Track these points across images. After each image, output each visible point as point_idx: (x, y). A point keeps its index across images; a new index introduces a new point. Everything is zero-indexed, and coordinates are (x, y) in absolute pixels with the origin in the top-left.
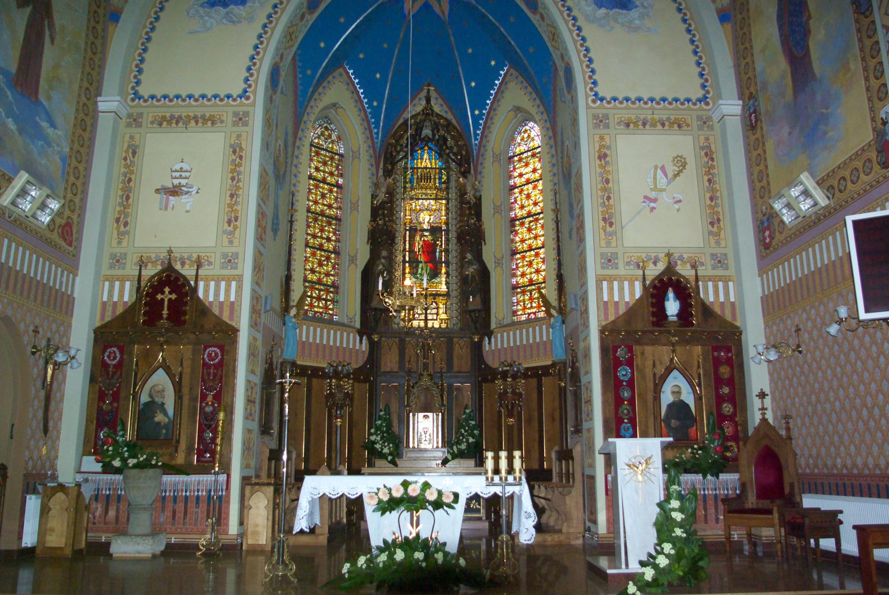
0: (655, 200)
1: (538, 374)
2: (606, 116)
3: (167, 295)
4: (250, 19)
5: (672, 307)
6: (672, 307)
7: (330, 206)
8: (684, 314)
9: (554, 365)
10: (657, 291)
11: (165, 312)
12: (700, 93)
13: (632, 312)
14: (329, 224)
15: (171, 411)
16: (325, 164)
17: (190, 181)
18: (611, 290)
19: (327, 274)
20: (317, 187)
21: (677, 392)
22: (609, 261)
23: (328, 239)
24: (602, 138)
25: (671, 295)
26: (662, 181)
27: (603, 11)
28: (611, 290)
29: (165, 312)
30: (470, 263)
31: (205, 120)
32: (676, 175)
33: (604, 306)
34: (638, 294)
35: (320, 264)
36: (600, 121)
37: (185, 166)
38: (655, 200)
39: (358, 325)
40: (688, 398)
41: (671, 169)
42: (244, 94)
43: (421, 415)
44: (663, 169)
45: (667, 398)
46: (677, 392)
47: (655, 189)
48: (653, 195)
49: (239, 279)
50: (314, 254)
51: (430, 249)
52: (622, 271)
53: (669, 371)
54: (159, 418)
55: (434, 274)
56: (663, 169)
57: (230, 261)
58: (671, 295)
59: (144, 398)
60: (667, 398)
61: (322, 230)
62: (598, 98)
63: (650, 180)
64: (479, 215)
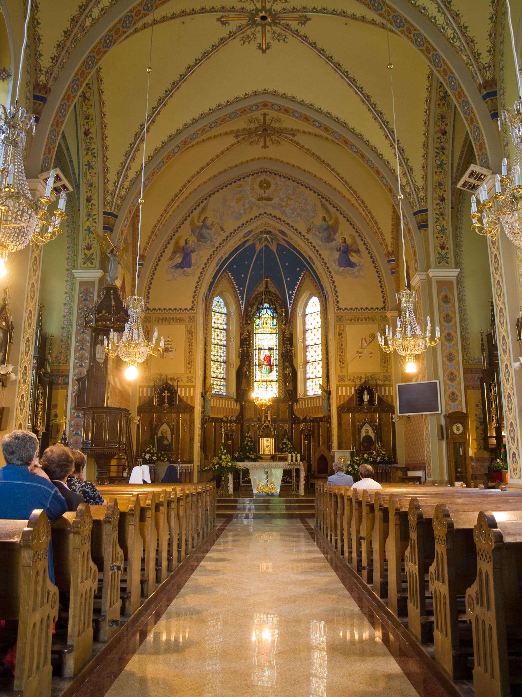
0: (361, 353)
1: (316, 420)
2: (342, 317)
3: (166, 394)
4: (193, 274)
5: (366, 398)
6: (366, 398)
7: (221, 340)
8: (371, 401)
9: (324, 417)
10: (360, 392)
11: (166, 401)
12: (382, 305)
13: (351, 399)
14: (221, 349)
15: (170, 440)
16: (218, 319)
17: (172, 346)
18: (342, 391)
19: (220, 373)
20: (215, 331)
21: (367, 432)
22: (342, 379)
23: (220, 356)
24: (340, 326)
25: (366, 393)
26: (364, 345)
27: (342, 268)
28: (342, 391)
29: (166, 401)
30: (287, 367)
31: (177, 320)
32: (370, 342)
33: (339, 397)
34: (353, 392)
35: (217, 369)
36: (339, 319)
37: (170, 340)
38: (361, 353)
39: (235, 397)
40: (371, 434)
41: (368, 340)
42: (192, 308)
43: (265, 439)
44: (365, 339)
45: (363, 434)
46: (367, 432)
47: (361, 348)
48: (360, 350)
49: (194, 387)
50: (214, 364)
51: (268, 359)
52: (347, 383)
53: (364, 424)
54: (166, 442)
55: (271, 371)
56: (365, 339)
57: (190, 379)
58: (366, 393)
59: (159, 434)
60: (363, 434)
61: (218, 352)
62: (339, 308)
63: (360, 344)
64: (291, 344)
